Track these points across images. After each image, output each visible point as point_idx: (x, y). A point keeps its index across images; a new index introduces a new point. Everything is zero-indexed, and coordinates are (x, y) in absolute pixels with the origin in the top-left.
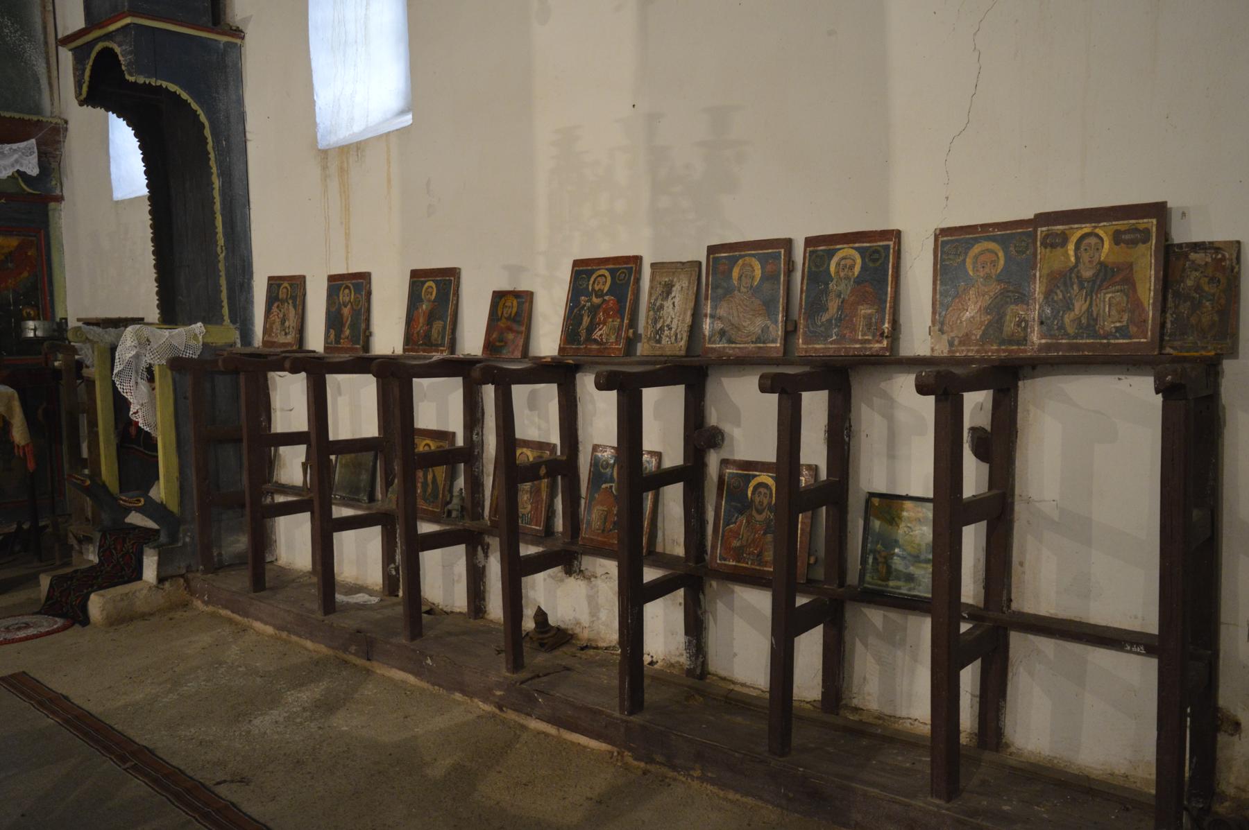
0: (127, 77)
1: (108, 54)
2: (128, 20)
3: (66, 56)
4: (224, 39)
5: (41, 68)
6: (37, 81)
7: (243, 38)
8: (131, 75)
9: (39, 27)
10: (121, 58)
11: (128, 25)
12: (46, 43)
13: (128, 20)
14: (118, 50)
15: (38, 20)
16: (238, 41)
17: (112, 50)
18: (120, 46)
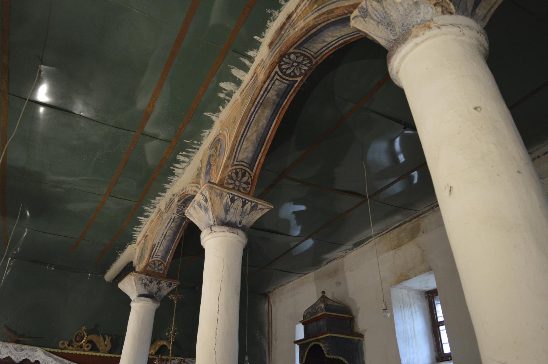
0: (326, 355)
1: (317, 347)
2: (328, 335)
3: (297, 347)
4: (357, 338)
5: (267, 348)
6: (265, 353)
7: (363, 337)
8: (329, 355)
9: (267, 333)
10: (323, 348)
11: (328, 336)
12: (269, 338)
13: (328, 335)
14: (321, 345)
15: (267, 330)
16: (361, 339)
17: (319, 345)
18: (323, 343)
